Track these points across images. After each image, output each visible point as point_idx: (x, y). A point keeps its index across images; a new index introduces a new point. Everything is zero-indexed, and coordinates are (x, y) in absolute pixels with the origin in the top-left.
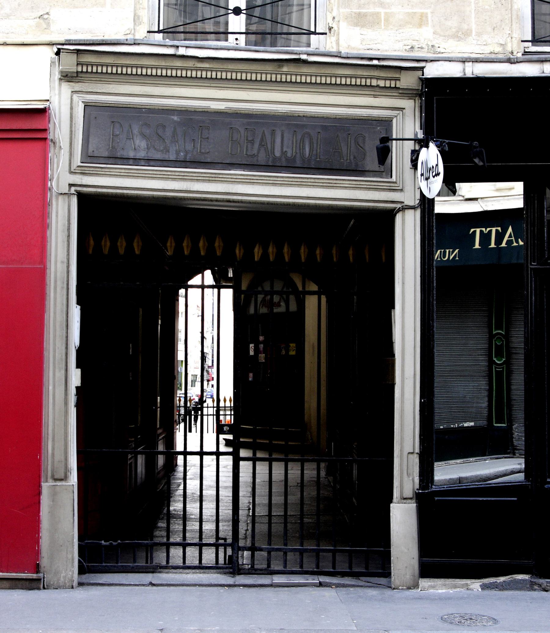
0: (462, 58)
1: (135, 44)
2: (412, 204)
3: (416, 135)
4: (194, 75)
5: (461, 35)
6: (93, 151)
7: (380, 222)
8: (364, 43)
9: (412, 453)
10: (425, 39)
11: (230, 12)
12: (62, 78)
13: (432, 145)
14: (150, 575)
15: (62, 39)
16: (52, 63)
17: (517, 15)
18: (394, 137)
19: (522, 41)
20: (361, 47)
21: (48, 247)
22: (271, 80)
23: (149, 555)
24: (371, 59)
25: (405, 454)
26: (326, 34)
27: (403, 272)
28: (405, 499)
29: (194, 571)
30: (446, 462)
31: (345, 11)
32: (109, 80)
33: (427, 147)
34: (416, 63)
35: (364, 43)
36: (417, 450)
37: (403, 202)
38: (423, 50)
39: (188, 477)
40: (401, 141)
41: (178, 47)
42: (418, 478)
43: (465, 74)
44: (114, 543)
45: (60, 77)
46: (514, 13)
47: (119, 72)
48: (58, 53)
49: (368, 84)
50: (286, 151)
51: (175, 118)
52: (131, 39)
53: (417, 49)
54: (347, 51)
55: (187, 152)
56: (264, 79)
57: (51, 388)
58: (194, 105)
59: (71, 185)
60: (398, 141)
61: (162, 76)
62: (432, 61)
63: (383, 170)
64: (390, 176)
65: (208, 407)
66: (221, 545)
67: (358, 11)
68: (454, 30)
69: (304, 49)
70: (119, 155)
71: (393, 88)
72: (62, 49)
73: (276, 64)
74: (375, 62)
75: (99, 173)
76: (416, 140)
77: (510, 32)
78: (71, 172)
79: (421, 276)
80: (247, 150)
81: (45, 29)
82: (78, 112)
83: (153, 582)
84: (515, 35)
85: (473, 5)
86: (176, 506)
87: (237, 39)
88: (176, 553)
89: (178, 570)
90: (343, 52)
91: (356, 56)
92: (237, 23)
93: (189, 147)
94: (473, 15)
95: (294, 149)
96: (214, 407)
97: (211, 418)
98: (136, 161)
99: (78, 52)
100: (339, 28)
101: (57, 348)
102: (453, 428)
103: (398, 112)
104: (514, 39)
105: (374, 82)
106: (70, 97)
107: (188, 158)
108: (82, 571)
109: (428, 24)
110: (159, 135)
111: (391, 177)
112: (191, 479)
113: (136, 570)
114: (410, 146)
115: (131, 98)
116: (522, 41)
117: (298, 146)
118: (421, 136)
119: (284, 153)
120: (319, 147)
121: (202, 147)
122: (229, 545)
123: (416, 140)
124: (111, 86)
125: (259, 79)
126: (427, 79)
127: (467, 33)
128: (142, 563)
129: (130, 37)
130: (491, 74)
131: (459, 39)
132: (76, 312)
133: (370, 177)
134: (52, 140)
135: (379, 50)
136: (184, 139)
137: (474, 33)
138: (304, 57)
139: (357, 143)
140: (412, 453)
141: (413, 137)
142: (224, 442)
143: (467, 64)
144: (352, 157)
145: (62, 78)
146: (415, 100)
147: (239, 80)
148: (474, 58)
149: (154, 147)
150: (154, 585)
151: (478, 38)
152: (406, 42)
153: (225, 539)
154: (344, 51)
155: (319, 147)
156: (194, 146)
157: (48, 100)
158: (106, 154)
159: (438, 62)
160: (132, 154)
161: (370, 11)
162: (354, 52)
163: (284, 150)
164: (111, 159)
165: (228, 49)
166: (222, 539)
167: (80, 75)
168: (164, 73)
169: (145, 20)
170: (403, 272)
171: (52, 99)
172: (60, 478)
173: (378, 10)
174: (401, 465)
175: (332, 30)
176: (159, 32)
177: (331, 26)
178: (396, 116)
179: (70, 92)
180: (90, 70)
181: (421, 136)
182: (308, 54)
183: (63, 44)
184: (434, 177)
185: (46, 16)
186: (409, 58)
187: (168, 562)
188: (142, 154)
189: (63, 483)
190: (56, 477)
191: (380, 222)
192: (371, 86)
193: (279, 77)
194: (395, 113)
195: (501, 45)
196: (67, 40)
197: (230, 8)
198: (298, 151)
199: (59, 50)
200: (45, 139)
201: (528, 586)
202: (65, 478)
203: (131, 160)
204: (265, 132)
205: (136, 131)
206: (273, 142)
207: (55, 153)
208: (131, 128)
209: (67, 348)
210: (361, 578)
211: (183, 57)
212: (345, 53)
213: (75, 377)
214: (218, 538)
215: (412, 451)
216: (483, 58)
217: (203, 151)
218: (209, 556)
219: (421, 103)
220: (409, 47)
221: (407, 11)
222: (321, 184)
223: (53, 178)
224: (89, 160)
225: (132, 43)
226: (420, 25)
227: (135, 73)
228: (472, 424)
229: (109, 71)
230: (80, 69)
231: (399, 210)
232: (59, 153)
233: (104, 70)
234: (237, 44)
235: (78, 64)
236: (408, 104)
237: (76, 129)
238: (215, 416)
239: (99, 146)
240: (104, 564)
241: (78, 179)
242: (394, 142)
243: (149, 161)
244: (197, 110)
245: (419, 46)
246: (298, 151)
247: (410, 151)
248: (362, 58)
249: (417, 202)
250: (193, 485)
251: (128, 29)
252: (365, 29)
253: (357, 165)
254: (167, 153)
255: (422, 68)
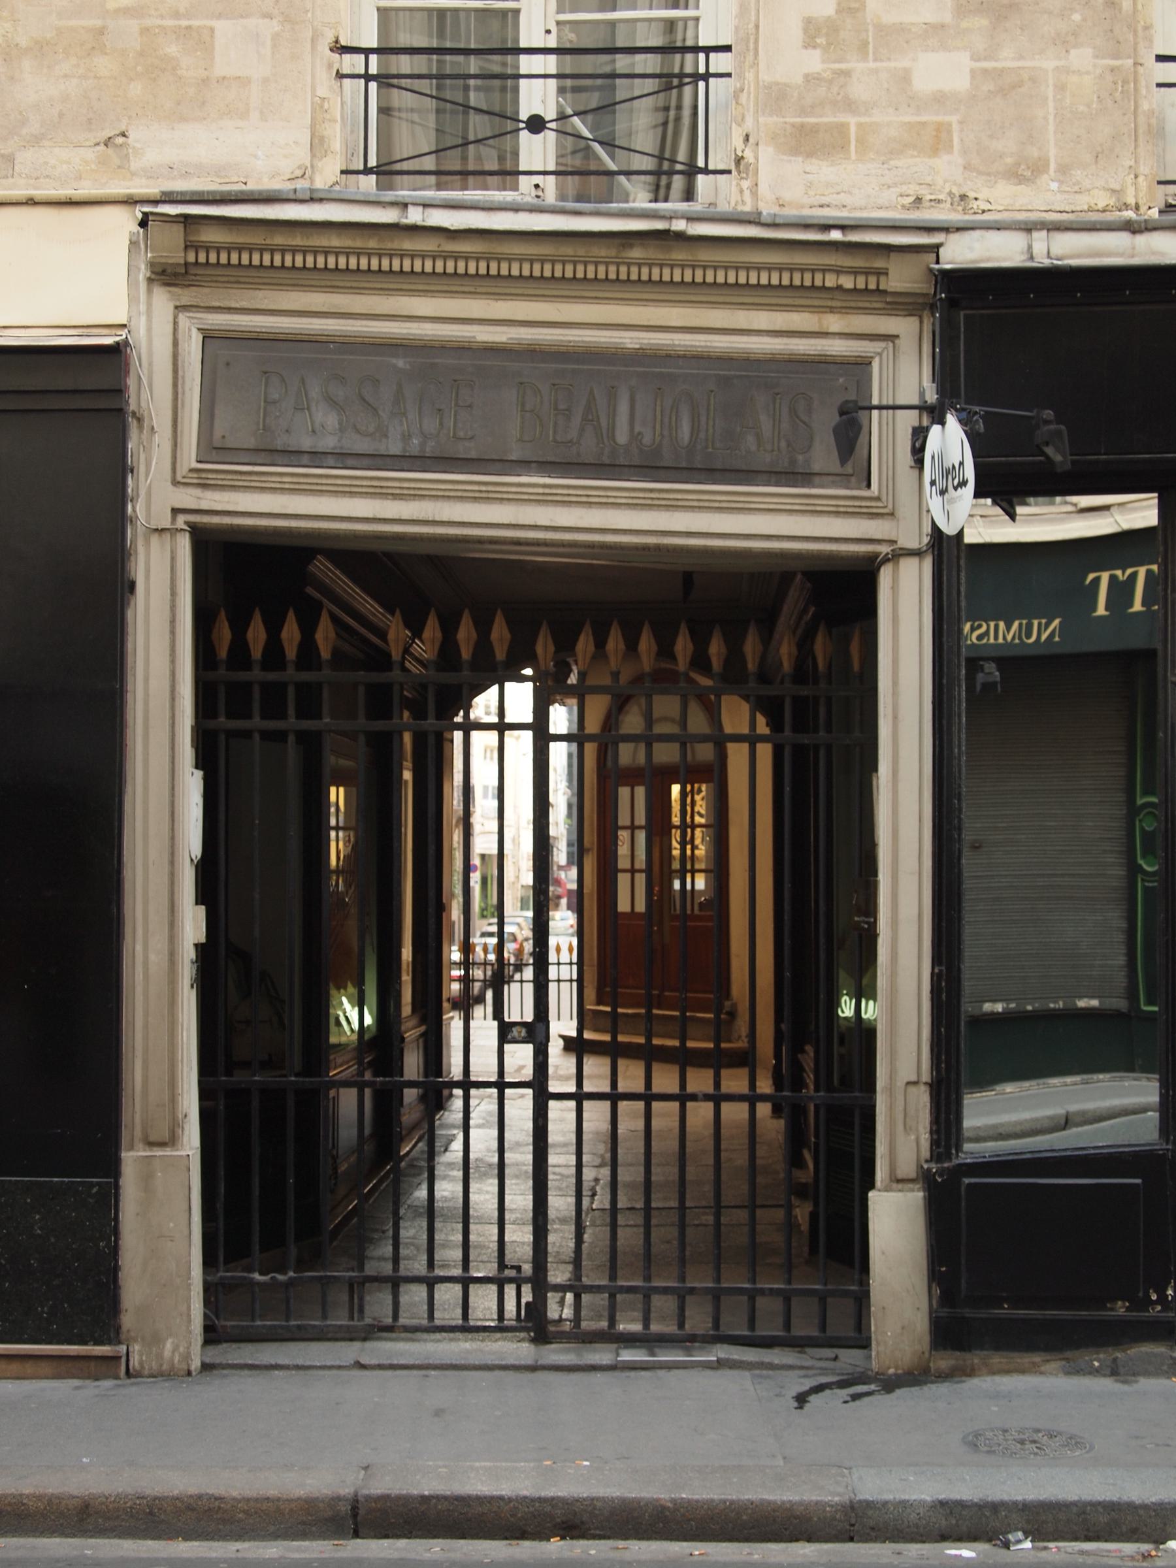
0: (1026, 223)
1: (312, 200)
2: (913, 544)
3: (922, 394)
4: (720, 279)
5: (1025, 172)
6: (223, 437)
7: (844, 591)
8: (812, 193)
9: (915, 1083)
10: (945, 181)
11: (522, 125)
12: (153, 276)
13: (951, 420)
14: (357, 1345)
15: (152, 189)
16: (133, 244)
17: (1149, 125)
18: (875, 401)
19: (1159, 183)
20: (807, 201)
21: (130, 646)
22: (477, 274)
23: (356, 1301)
24: (827, 228)
25: (900, 1083)
26: (729, 172)
27: (895, 694)
28: (899, 1181)
29: (451, 1335)
30: (1041, 1081)
31: (770, 121)
32: (257, 280)
33: (942, 423)
34: (925, 235)
35: (812, 193)
36: (926, 1077)
37: (896, 542)
38: (942, 206)
39: (472, 1122)
40: (891, 411)
41: (405, 205)
42: (927, 1136)
43: (1032, 258)
44: (280, 1277)
45: (148, 274)
46: (1142, 119)
47: (277, 262)
48: (143, 224)
49: (818, 283)
50: (639, 433)
51: (400, 363)
52: (303, 190)
53: (928, 204)
54: (775, 210)
55: (425, 437)
56: (808, 283)
57: (139, 948)
58: (440, 333)
59: (176, 511)
60: (884, 412)
61: (380, 270)
62: (958, 229)
63: (850, 471)
64: (865, 484)
65: (559, 964)
66: (511, 1280)
67: (799, 120)
68: (1009, 160)
69: (683, 206)
70: (279, 444)
71: (872, 291)
72: (152, 213)
73: (617, 241)
74: (836, 235)
75: (237, 483)
76: (923, 408)
77: (1132, 163)
78: (175, 483)
79: (933, 703)
80: (555, 432)
81: (119, 167)
82: (189, 353)
83: (362, 1362)
84: (1144, 169)
85: (1051, 104)
86: (448, 1189)
87: (537, 186)
88: (414, 1295)
89: (419, 1335)
90: (764, 213)
91: (793, 221)
92: (537, 151)
93: (430, 424)
94: (1051, 128)
95: (658, 427)
96: (571, 964)
97: (565, 986)
98: (316, 457)
99: (186, 219)
100: (757, 159)
101: (151, 862)
102: (1054, 1010)
103: (882, 344)
104: (1141, 179)
105: (831, 281)
106: (171, 319)
107: (428, 449)
108: (212, 1335)
109: (952, 147)
110: (364, 400)
111: (869, 486)
112: (479, 1126)
113: (330, 1335)
114: (907, 420)
115: (304, 320)
116: (1159, 183)
117: (666, 420)
118: (932, 397)
119: (635, 437)
120: (711, 423)
121: (460, 425)
122: (527, 1280)
123: (923, 408)
124: (260, 294)
125: (461, 270)
126: (945, 273)
127: (1038, 168)
128: (340, 1320)
129: (301, 184)
130: (1090, 256)
131: (1020, 179)
132: (193, 786)
133: (822, 487)
134: (134, 413)
135: (844, 206)
136: (420, 408)
137: (1052, 166)
138: (679, 225)
139: (793, 412)
140: (915, 1083)
141: (915, 401)
142: (561, 1042)
143: (1035, 234)
144: (783, 444)
145: (153, 276)
146: (921, 317)
147: (450, 275)
148: (1052, 222)
149: (355, 427)
150: (363, 1367)
151: (1061, 178)
152: (904, 189)
153: (518, 1268)
154: (768, 209)
155: (711, 423)
156: (441, 424)
157: (125, 326)
158: (251, 443)
159: (971, 232)
160: (307, 443)
161: (825, 120)
162: (790, 212)
163: (637, 429)
164: (263, 454)
165: (516, 208)
166: (513, 1267)
167: (193, 271)
168: (407, 267)
169: (337, 145)
170: (895, 694)
171: (132, 323)
172: (160, 1140)
173: (842, 118)
174: (891, 1108)
175: (742, 163)
176: (367, 171)
177: (740, 154)
178: (880, 354)
179: (172, 308)
180: (256, 260)
181: (932, 397)
182: (690, 219)
183: (156, 202)
184: (956, 489)
185: (120, 140)
186: (908, 224)
187: (396, 1316)
188: (329, 443)
189: (168, 1152)
190: (152, 1139)
191: (844, 591)
192: (824, 288)
193: (666, 273)
194: (878, 346)
195: (1113, 191)
196: (164, 193)
197: (521, 118)
198: (666, 433)
199: (145, 215)
200: (120, 410)
201: (1165, 1368)
202: (172, 1140)
203: (306, 456)
204: (595, 392)
205: (315, 392)
206: (613, 414)
207: (140, 442)
208: (303, 383)
209: (172, 863)
210: (808, 1350)
211: (414, 229)
212: (769, 214)
213: (193, 925)
214: (502, 1265)
215: (914, 1078)
216: (1072, 222)
217: (461, 434)
218: (484, 1302)
219: (933, 324)
220: (911, 199)
221: (907, 119)
222: (717, 505)
223: (138, 496)
224: (214, 455)
225: (307, 197)
226: (935, 151)
227: (376, 268)
228: (1095, 1003)
229: (256, 262)
230: (191, 258)
231: (886, 560)
232: (150, 441)
233: (245, 260)
234: (538, 197)
235: (186, 247)
236: (904, 326)
237: (187, 389)
238: (575, 984)
239: (235, 427)
240: (259, 1323)
241: (189, 498)
242: (875, 413)
243: (343, 458)
244: (448, 345)
245: (933, 197)
246: (666, 433)
247: (910, 431)
248: (807, 226)
249: (926, 540)
250: (483, 1140)
251: (299, 167)
252: (814, 161)
253: (793, 462)
254: (384, 440)
255: (936, 248)
